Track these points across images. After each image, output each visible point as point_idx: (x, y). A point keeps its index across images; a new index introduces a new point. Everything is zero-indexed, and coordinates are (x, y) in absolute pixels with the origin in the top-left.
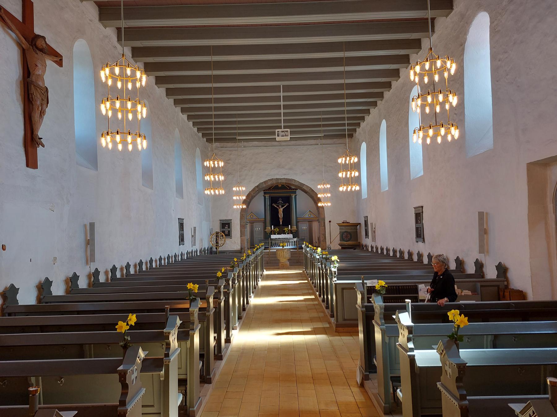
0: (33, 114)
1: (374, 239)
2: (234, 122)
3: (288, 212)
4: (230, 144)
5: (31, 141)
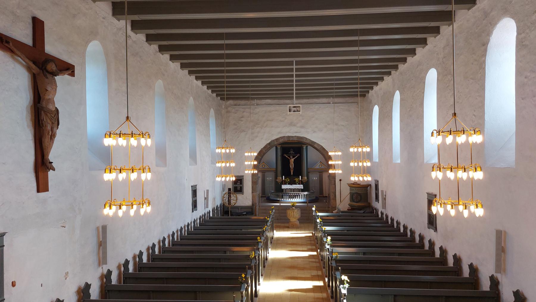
0: (43, 139)
1: (384, 206)
2: (248, 87)
3: (299, 162)
4: (243, 102)
5: (42, 165)
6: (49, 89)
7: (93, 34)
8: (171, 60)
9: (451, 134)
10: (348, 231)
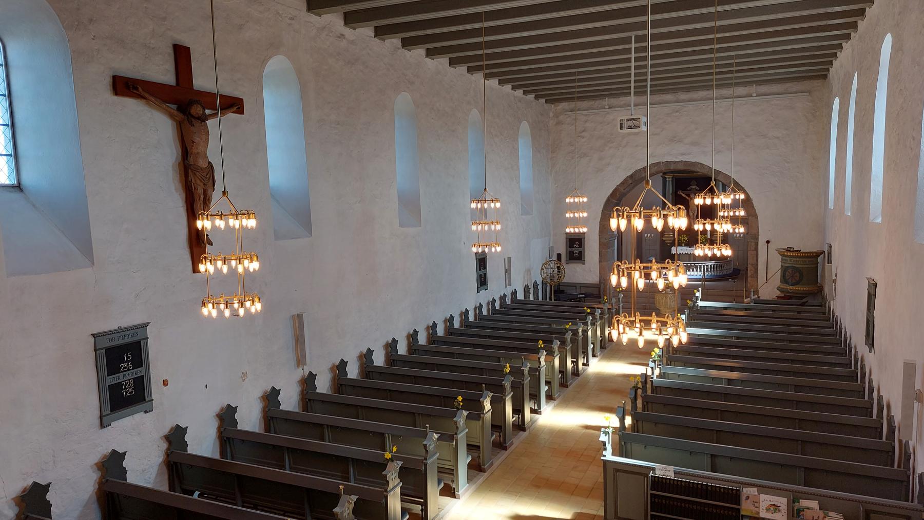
6: (197, 139)
7: (274, 47)
8: (427, 56)
9: (640, 217)
10: (738, 338)
